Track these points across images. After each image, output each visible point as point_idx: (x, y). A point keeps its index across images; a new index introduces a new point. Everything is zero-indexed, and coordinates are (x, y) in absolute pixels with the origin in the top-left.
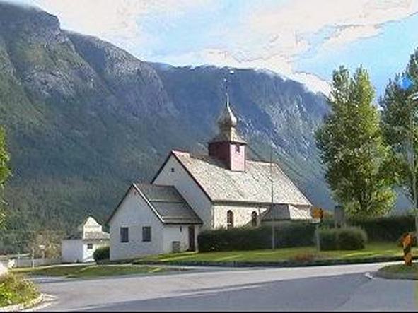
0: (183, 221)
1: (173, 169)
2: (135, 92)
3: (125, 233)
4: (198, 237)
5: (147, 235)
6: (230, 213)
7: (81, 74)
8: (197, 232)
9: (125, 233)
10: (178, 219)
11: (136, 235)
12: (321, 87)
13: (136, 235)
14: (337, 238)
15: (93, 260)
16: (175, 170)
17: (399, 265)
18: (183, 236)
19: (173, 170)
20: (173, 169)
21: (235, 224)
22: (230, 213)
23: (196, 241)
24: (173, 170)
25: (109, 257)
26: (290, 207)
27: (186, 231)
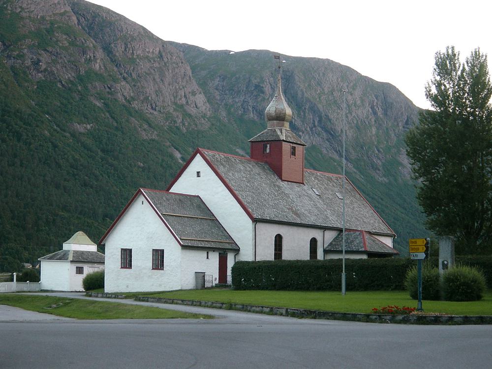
0: (213, 245)
1: (198, 173)
2: (154, 79)
3: (127, 258)
4: (233, 269)
5: (159, 259)
6: (279, 239)
7: (94, 65)
8: (230, 263)
9: (127, 258)
10: (152, 324)
11: (142, 260)
12: (417, 89)
13: (142, 260)
14: (442, 279)
15: (84, 291)
16: (201, 174)
17: (359, 260)
18: (210, 266)
19: (198, 174)
20: (198, 173)
21: (287, 256)
22: (279, 239)
23: (229, 273)
24: (198, 174)
25: (103, 287)
26: (365, 234)
27: (215, 258)
